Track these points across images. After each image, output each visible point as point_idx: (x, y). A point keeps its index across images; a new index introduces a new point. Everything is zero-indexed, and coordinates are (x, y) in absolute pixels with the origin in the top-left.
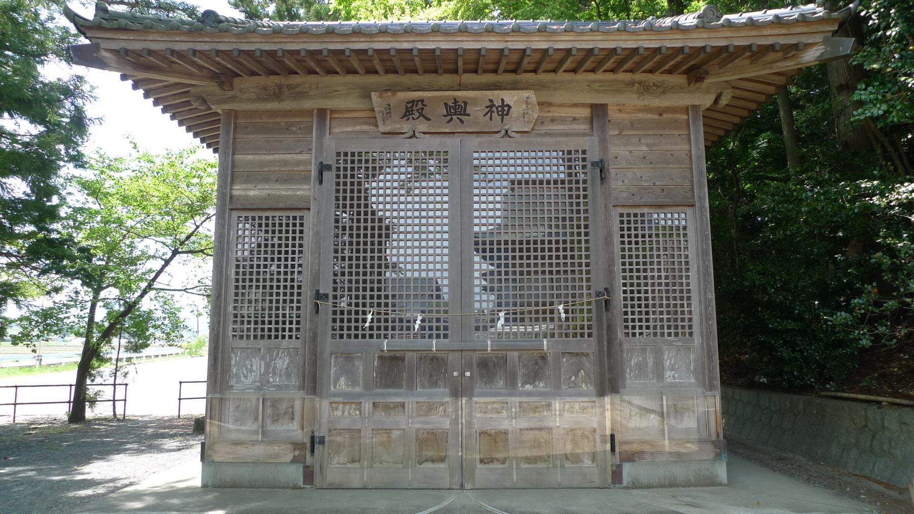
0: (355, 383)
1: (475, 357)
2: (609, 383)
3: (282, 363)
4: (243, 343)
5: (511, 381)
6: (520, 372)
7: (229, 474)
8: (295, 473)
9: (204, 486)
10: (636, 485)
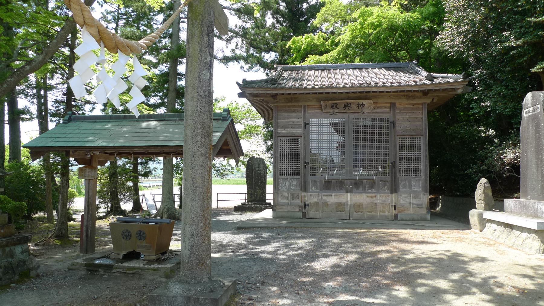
0: (317, 189)
1: (353, 181)
2: (394, 189)
3: (295, 183)
4: (283, 177)
5: (364, 189)
6: (367, 186)
7: (280, 214)
8: (300, 214)
9: (273, 218)
10: (402, 220)
